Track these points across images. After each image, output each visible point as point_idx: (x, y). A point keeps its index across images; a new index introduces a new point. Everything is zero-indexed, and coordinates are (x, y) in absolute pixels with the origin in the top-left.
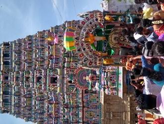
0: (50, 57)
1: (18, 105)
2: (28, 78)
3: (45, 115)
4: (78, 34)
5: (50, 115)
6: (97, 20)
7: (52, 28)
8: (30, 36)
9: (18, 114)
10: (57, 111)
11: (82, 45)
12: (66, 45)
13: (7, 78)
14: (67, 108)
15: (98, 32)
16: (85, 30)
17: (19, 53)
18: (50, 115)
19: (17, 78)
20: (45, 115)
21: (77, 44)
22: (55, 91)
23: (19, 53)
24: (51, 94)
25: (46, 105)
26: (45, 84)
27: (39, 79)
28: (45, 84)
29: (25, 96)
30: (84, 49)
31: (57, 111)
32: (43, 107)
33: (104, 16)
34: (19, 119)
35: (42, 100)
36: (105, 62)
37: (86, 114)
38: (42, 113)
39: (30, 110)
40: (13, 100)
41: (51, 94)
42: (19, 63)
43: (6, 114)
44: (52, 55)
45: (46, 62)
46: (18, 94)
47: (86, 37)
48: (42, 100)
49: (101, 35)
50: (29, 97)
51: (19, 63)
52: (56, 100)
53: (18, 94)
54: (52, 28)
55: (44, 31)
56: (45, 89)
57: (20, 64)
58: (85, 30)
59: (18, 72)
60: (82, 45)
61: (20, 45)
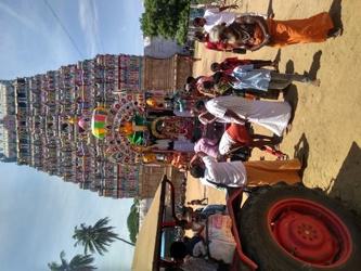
0: (78, 100)
1: (39, 156)
2: (50, 125)
3: (74, 169)
4: (111, 120)
5: (79, 169)
6: (136, 103)
7: (80, 63)
8: (50, 72)
9: (40, 167)
10: (88, 164)
11: (116, 136)
12: (95, 132)
13: (24, 123)
14: (100, 161)
15: (138, 121)
16: (119, 117)
17: (38, 93)
18: (79, 169)
19: (37, 124)
20: (74, 169)
21: (110, 135)
22: (85, 142)
23: (38, 93)
24: (80, 144)
25: (74, 158)
26: (72, 133)
27: (64, 126)
28: (72, 133)
29: (48, 146)
30: (119, 142)
31: (88, 164)
32: (70, 160)
33: (147, 98)
34: (41, 172)
35: (69, 151)
36: (145, 160)
37: (121, 170)
38: (70, 166)
39: (55, 162)
40: (34, 150)
41: (80, 144)
42: (38, 106)
43: (24, 166)
44: (80, 98)
45: (73, 107)
46: (39, 144)
47: (122, 126)
48: (69, 151)
49: (141, 125)
50: (53, 147)
51: (38, 106)
52: (87, 152)
53: (39, 144)
54: (80, 63)
55: (70, 66)
56: (73, 139)
57: (40, 107)
58: (119, 117)
59: (37, 117)
60: (116, 136)
61: (39, 83)
